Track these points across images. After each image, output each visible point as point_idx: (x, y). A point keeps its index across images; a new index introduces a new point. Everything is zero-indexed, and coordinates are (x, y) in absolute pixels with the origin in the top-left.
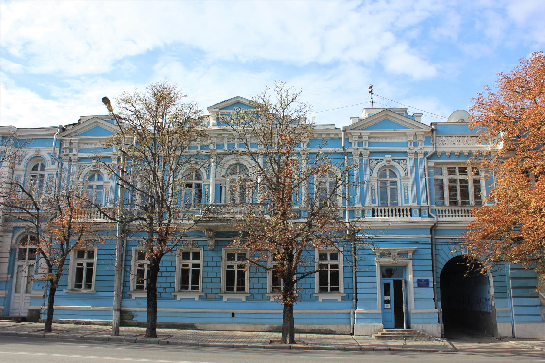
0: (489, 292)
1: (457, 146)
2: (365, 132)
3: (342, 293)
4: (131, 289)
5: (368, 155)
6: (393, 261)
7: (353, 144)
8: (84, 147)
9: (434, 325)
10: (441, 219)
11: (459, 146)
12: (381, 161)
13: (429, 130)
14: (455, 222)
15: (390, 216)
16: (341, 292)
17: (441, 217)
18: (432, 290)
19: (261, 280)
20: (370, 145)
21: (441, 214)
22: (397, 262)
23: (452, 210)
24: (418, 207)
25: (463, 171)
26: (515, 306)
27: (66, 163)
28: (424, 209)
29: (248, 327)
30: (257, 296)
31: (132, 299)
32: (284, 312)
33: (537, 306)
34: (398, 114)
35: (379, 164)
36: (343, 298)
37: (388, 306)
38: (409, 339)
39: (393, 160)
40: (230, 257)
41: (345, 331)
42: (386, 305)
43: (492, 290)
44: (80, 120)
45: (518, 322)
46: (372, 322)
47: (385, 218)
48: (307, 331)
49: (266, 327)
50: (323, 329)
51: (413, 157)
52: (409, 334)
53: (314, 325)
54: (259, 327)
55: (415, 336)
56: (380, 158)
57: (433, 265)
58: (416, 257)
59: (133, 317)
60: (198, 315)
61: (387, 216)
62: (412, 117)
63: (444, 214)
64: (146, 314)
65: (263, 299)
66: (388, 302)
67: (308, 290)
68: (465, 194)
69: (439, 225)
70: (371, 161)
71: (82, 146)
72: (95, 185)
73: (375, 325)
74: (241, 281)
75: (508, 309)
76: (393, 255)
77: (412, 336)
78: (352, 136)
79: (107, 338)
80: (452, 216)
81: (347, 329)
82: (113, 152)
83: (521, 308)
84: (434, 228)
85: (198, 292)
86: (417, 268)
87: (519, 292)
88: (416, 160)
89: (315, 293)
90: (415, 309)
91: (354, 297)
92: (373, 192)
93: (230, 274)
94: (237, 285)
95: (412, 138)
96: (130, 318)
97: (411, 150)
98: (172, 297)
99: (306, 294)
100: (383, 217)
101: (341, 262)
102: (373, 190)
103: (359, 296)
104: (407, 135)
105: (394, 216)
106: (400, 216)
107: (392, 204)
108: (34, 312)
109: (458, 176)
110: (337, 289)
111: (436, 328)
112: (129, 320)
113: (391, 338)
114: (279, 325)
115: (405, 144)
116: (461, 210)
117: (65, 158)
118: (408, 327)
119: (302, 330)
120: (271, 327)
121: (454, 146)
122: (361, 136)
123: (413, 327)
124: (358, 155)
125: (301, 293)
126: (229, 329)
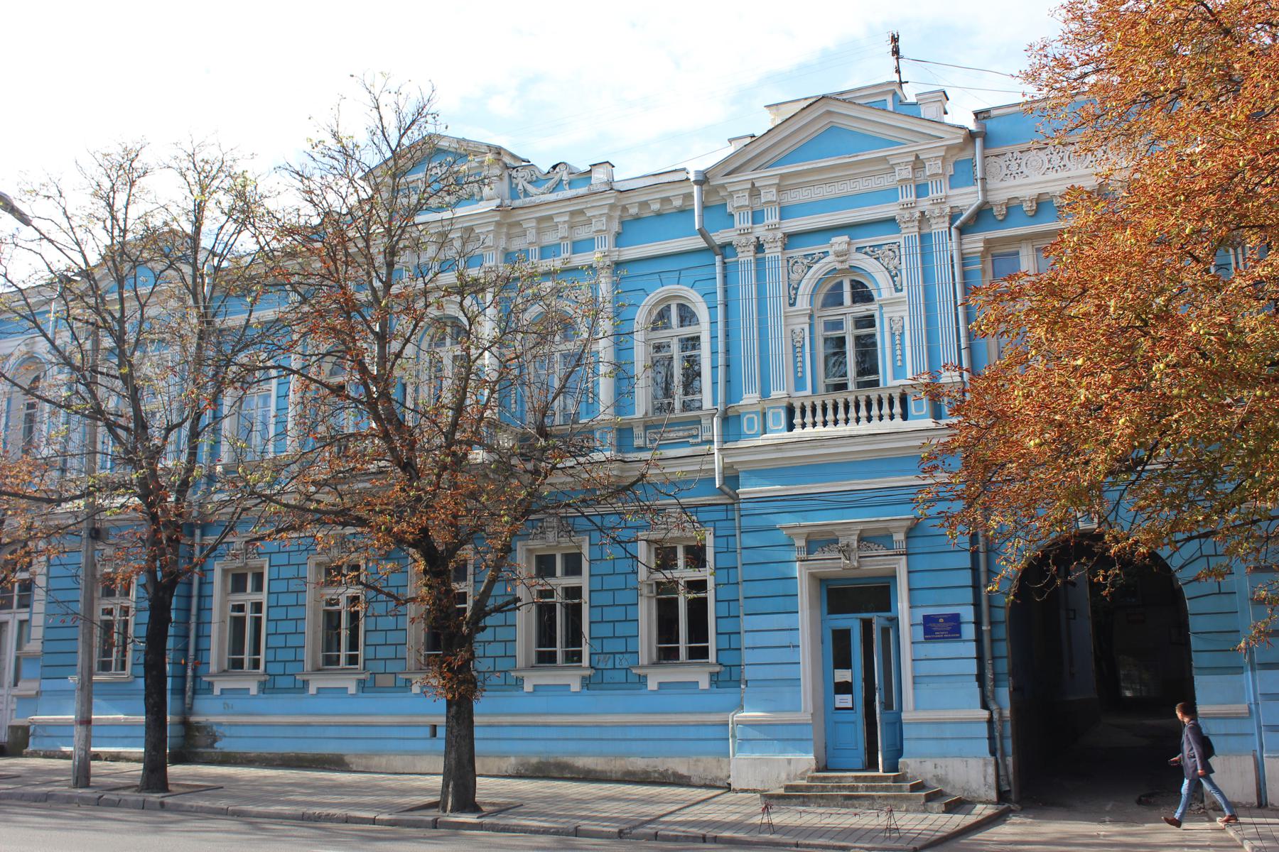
1: (1065, 174)
2: (766, 177)
3: (712, 664)
4: (213, 668)
5: (779, 244)
9: (972, 762)
12: (820, 259)
15: (841, 422)
18: (971, 649)
20: (785, 213)
22: (856, 564)
28: (749, 413)
31: (525, 690)
35: (816, 267)
37: (844, 700)
38: (860, 805)
41: (717, 778)
42: (838, 697)
46: (783, 752)
47: (827, 429)
48: (614, 776)
49: (510, 764)
50: (655, 771)
52: (867, 789)
53: (631, 759)
55: (880, 797)
56: (816, 250)
58: (919, 545)
59: (215, 741)
60: (352, 732)
61: (830, 424)
66: (844, 688)
67: (621, 656)
70: (791, 262)
71: (795, 197)
72: (675, 340)
73: (789, 761)
75: (1242, 708)
76: (845, 542)
77: (872, 797)
82: (901, 200)
86: (920, 580)
88: (925, 238)
89: (516, 670)
90: (916, 709)
92: (799, 355)
95: (907, 173)
97: (908, 211)
98: (299, 685)
99: (614, 668)
100: (819, 428)
102: (798, 350)
104: (892, 167)
105: (852, 422)
107: (861, 385)
108: (20, 732)
112: (207, 747)
114: (543, 760)
115: (888, 195)
118: (892, 766)
119: (602, 772)
120: (522, 765)
121: (1052, 175)
122: (754, 191)
124: (752, 248)
125: (601, 666)
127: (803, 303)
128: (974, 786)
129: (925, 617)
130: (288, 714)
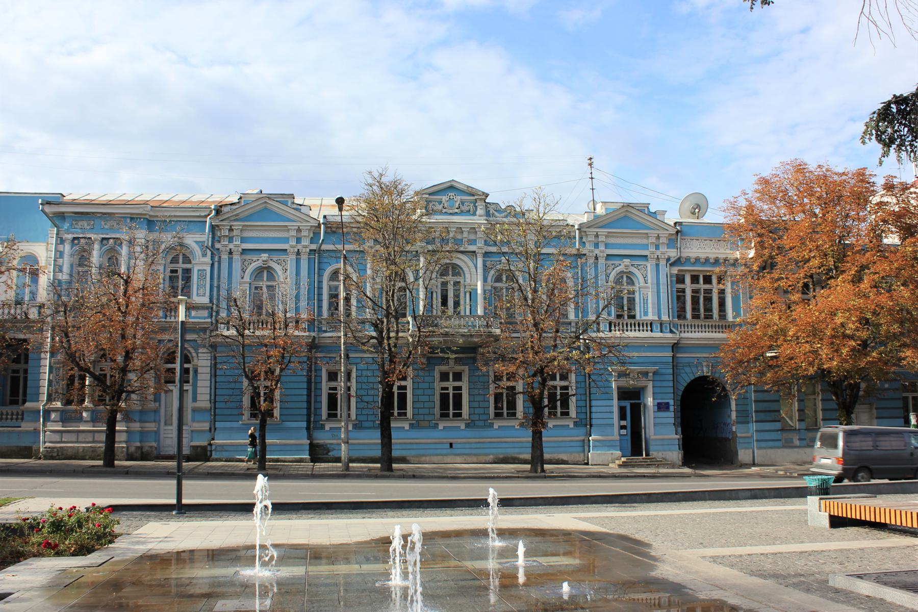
0: (730, 416)
1: (703, 251)
3: (574, 418)
6: (631, 382)
7: (587, 245)
8: (248, 236)
10: (683, 335)
11: (706, 251)
13: (673, 231)
14: (698, 339)
16: (465, 418)
17: (683, 332)
18: (672, 414)
19: (482, 404)
20: (243, 240)
21: (683, 329)
23: (695, 325)
24: (660, 322)
25: (707, 280)
26: (757, 431)
27: (225, 257)
29: (469, 459)
30: (477, 423)
31: (440, 428)
32: (533, 439)
33: (778, 430)
34: (277, 201)
36: (576, 424)
37: (624, 432)
39: (632, 265)
40: (444, 377)
42: (622, 431)
43: (734, 415)
44: (241, 198)
45: (759, 448)
46: (609, 450)
51: (654, 262)
52: (651, 462)
54: (482, 458)
56: (617, 262)
57: (673, 387)
58: (657, 378)
59: (329, 452)
62: (654, 215)
63: (686, 329)
64: (380, 447)
65: (485, 427)
68: (708, 309)
69: (681, 342)
74: (458, 404)
75: (749, 435)
78: (587, 235)
79: (343, 474)
80: (695, 332)
81: (580, 457)
82: (290, 244)
83: (762, 433)
84: (676, 345)
85: (407, 419)
86: (658, 390)
87: (762, 416)
88: (657, 265)
90: (655, 435)
91: (588, 423)
93: (444, 398)
94: (453, 410)
96: (325, 452)
101: (464, 384)
103: (594, 422)
106: (639, 330)
108: (199, 449)
109: (702, 286)
110: (514, 414)
111: (676, 455)
112: (324, 455)
113: (633, 466)
115: (645, 247)
116: (705, 325)
117: (223, 249)
120: (496, 458)
121: (700, 250)
122: (597, 236)
123: (653, 454)
126: (448, 462)
127: (247, 278)
128: (675, 460)
129: (658, 403)
130: (372, 439)
